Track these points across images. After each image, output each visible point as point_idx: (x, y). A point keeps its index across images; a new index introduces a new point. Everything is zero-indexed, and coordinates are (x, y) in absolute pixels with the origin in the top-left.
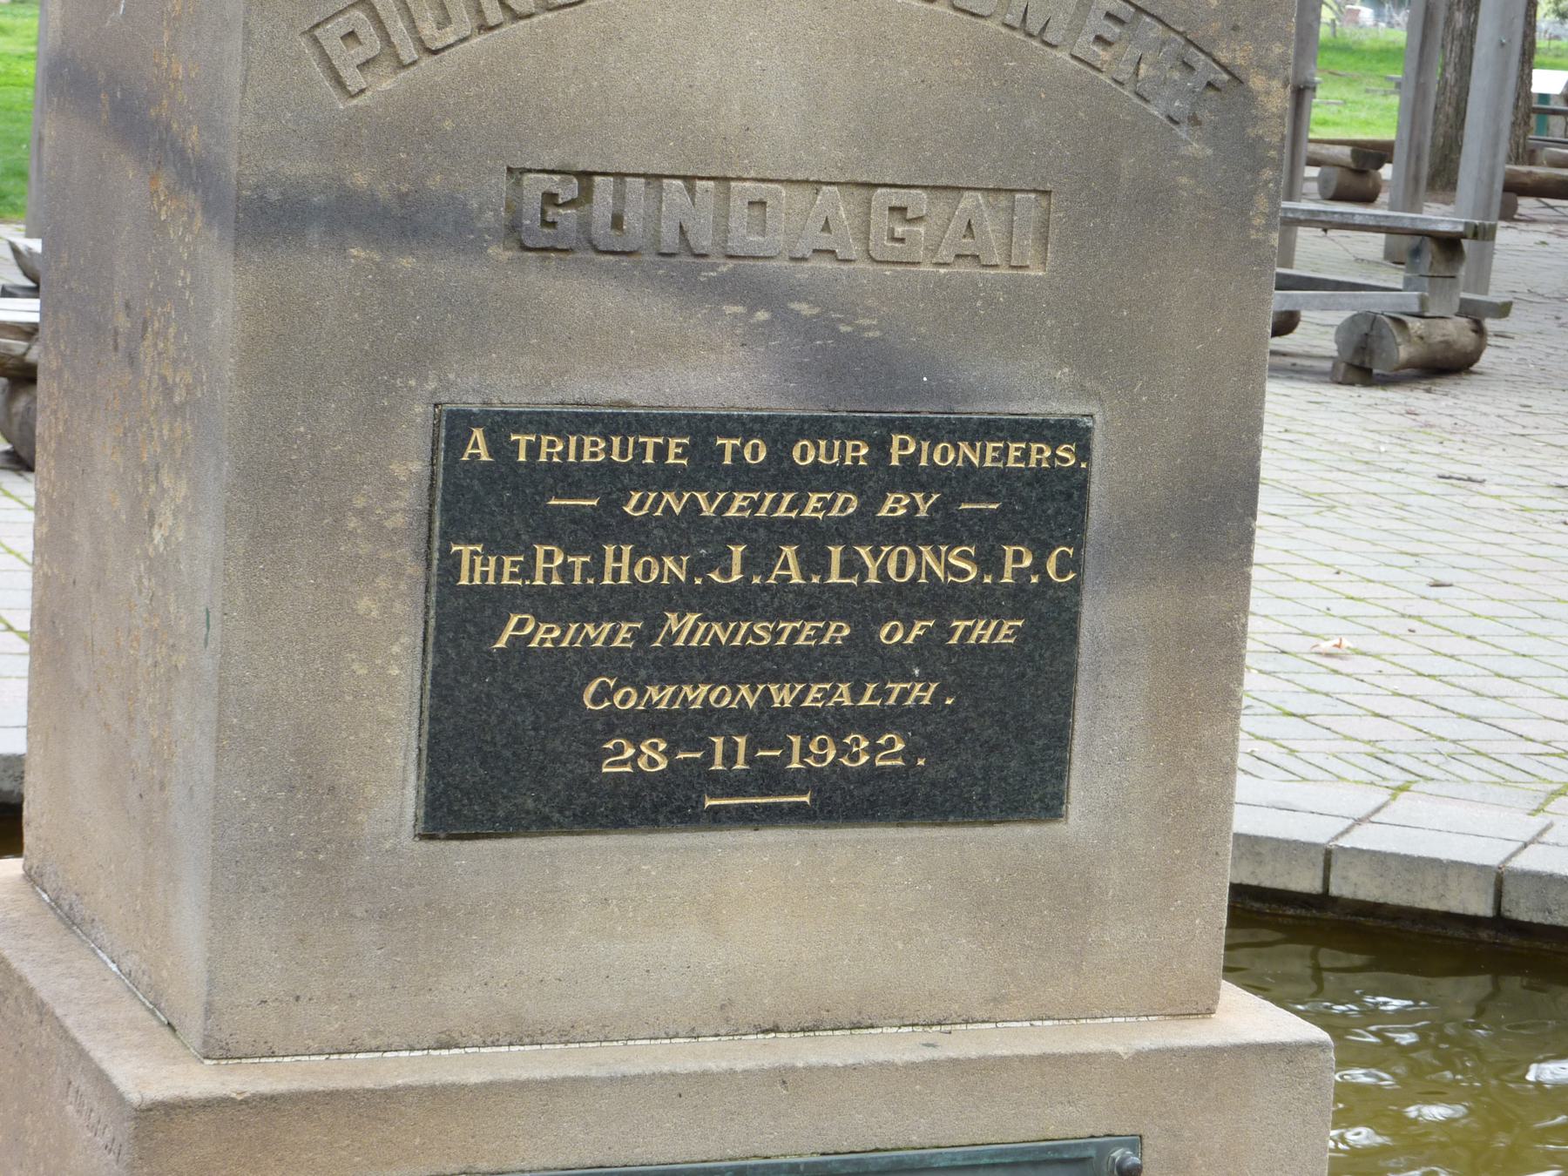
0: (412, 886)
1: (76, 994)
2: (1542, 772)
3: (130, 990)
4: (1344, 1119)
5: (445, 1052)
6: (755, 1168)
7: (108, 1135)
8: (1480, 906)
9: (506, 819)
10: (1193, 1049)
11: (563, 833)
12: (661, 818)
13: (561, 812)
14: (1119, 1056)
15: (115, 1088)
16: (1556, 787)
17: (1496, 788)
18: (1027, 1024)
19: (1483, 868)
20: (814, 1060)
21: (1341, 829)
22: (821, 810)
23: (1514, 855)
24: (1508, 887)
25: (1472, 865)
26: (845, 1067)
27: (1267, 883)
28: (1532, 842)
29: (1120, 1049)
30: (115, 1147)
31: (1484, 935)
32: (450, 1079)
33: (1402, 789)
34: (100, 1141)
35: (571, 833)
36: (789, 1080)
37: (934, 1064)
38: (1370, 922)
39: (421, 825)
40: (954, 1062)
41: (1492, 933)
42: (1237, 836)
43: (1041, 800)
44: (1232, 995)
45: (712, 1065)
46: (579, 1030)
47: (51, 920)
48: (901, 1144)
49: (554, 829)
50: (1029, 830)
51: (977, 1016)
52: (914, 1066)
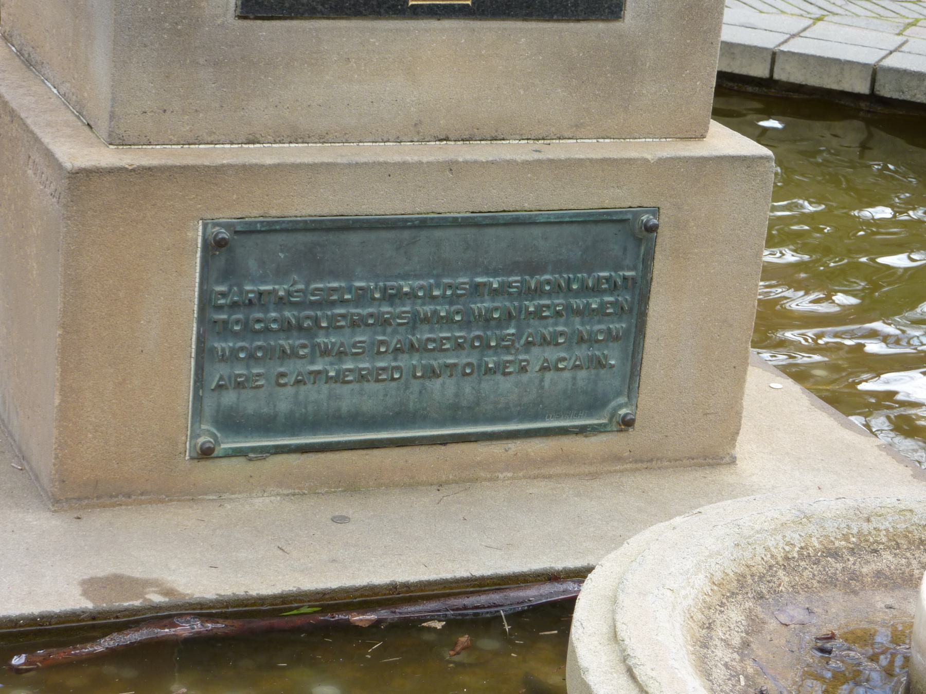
0: (233, 46)
1: (34, 106)
2: (903, 11)
3: (65, 104)
4: (772, 242)
5: (251, 146)
6: (432, 219)
7: (53, 187)
8: (862, 88)
9: (290, 8)
10: (691, 158)
11: (324, 18)
12: (382, 11)
13: (323, 5)
14: (648, 161)
15: (56, 160)
16: (910, 21)
17: (875, 20)
18: (595, 141)
19: (865, 65)
20: (469, 157)
21: (782, 40)
22: (478, 10)
23: (884, 58)
24: (879, 77)
25: (859, 63)
26: (487, 162)
27: (737, 71)
28: (895, 50)
29: (649, 157)
30: (57, 195)
31: (863, 105)
32: (254, 161)
33: (820, 19)
34: (48, 191)
35: (328, 18)
36: (454, 168)
37: (539, 162)
38: (796, 96)
39: (239, 10)
40: (551, 161)
41: (868, 104)
42: (722, 42)
43: (609, 8)
44: (717, 129)
45: (409, 159)
46: (331, 136)
47: (17, 62)
48: (518, 208)
49: (318, 15)
50: (601, 26)
51: (566, 135)
52: (526, 163)
